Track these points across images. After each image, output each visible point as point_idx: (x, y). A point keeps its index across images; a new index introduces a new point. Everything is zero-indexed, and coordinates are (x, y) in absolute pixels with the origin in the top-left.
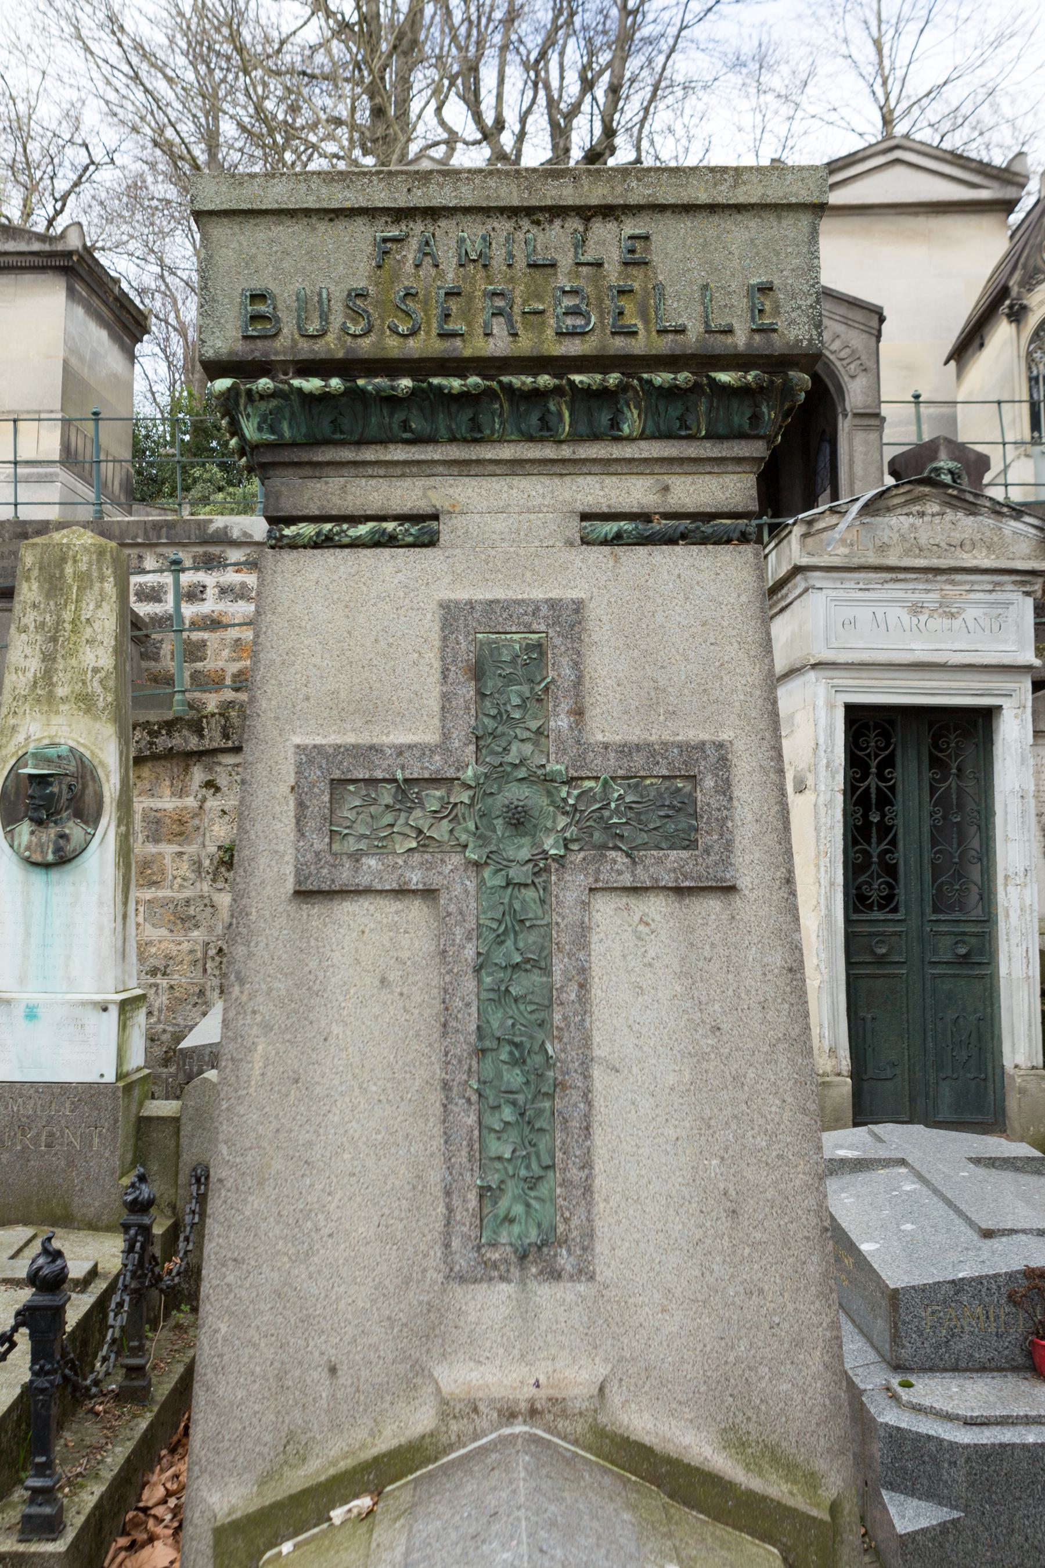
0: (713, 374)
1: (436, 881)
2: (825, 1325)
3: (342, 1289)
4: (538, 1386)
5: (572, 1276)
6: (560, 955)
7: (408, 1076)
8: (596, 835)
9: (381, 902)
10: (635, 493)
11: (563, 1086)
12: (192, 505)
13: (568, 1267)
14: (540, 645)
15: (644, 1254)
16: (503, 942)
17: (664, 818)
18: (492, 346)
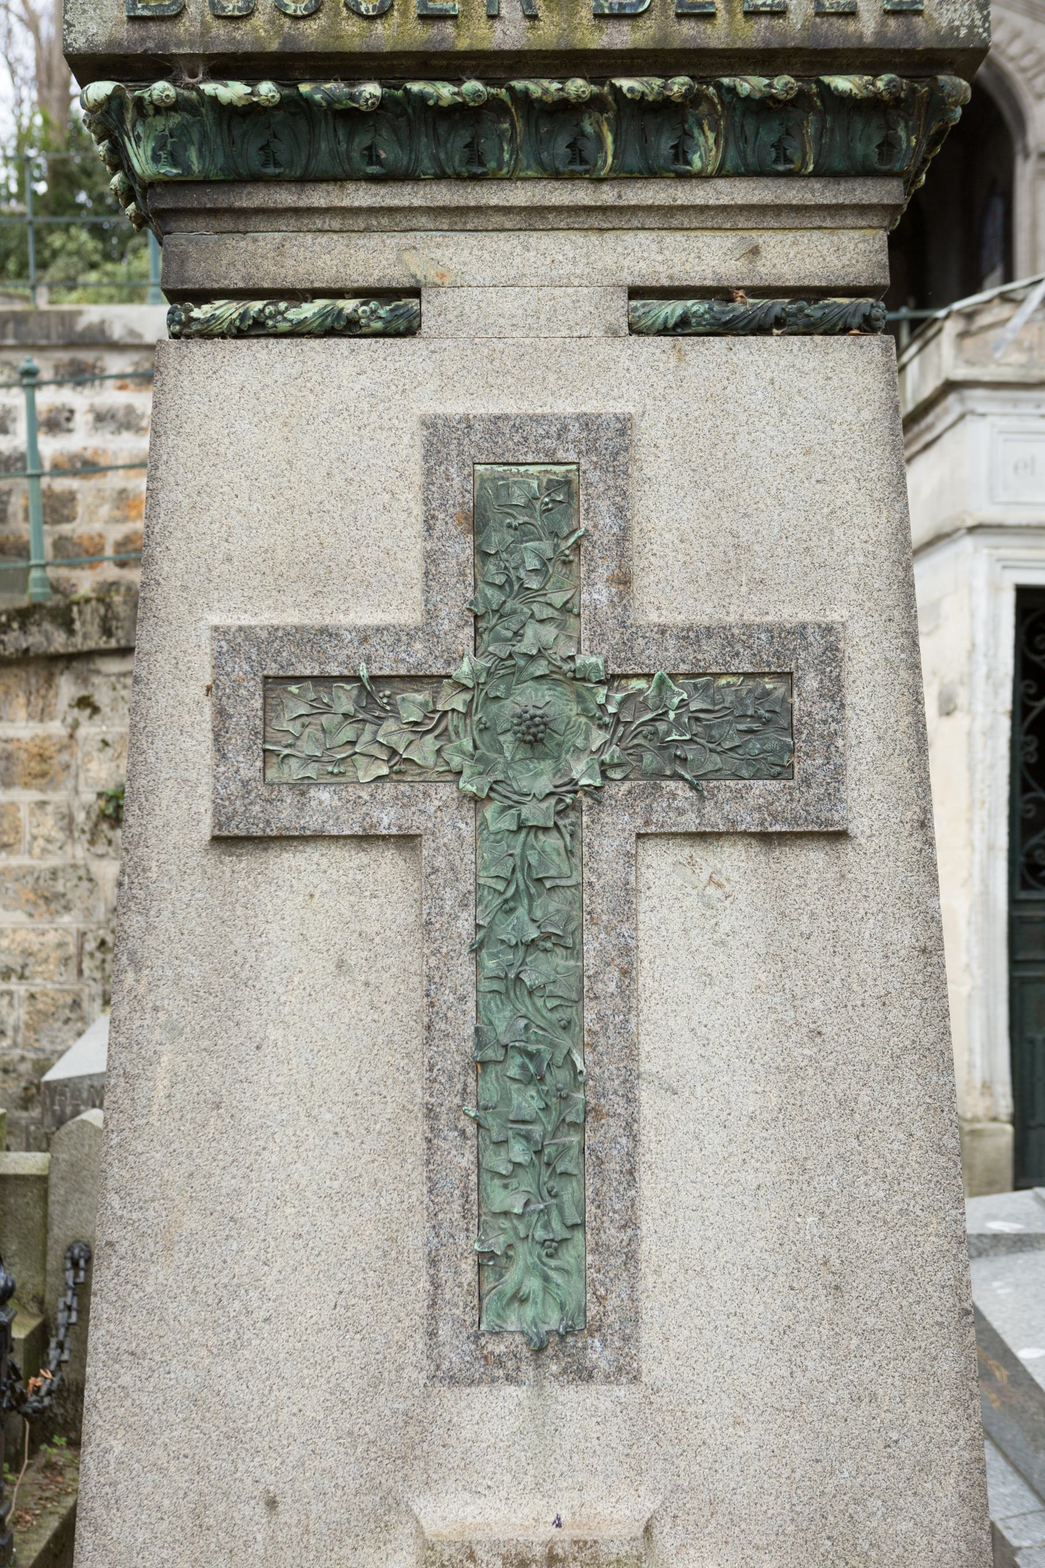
0: (826, 79)
1: (417, 823)
2: (961, 1442)
3: (284, 1393)
4: (559, 1525)
5: (607, 1376)
6: (595, 929)
7: (377, 1098)
8: (648, 758)
9: (338, 853)
10: (707, 257)
11: (598, 1113)
12: (51, 287)
13: (603, 1364)
14: (568, 482)
15: (709, 1346)
16: (512, 910)
17: (744, 733)
18: (499, 34)
